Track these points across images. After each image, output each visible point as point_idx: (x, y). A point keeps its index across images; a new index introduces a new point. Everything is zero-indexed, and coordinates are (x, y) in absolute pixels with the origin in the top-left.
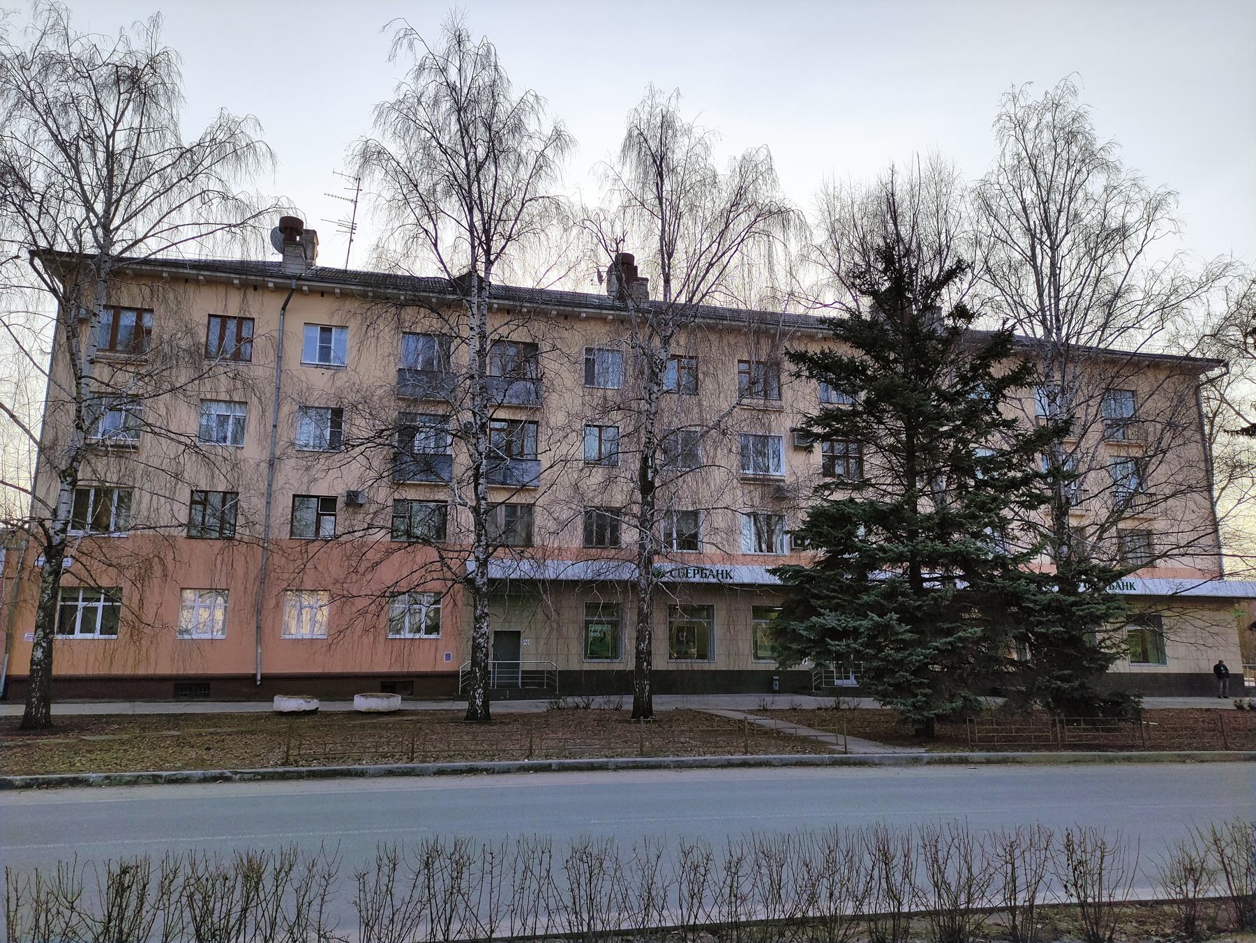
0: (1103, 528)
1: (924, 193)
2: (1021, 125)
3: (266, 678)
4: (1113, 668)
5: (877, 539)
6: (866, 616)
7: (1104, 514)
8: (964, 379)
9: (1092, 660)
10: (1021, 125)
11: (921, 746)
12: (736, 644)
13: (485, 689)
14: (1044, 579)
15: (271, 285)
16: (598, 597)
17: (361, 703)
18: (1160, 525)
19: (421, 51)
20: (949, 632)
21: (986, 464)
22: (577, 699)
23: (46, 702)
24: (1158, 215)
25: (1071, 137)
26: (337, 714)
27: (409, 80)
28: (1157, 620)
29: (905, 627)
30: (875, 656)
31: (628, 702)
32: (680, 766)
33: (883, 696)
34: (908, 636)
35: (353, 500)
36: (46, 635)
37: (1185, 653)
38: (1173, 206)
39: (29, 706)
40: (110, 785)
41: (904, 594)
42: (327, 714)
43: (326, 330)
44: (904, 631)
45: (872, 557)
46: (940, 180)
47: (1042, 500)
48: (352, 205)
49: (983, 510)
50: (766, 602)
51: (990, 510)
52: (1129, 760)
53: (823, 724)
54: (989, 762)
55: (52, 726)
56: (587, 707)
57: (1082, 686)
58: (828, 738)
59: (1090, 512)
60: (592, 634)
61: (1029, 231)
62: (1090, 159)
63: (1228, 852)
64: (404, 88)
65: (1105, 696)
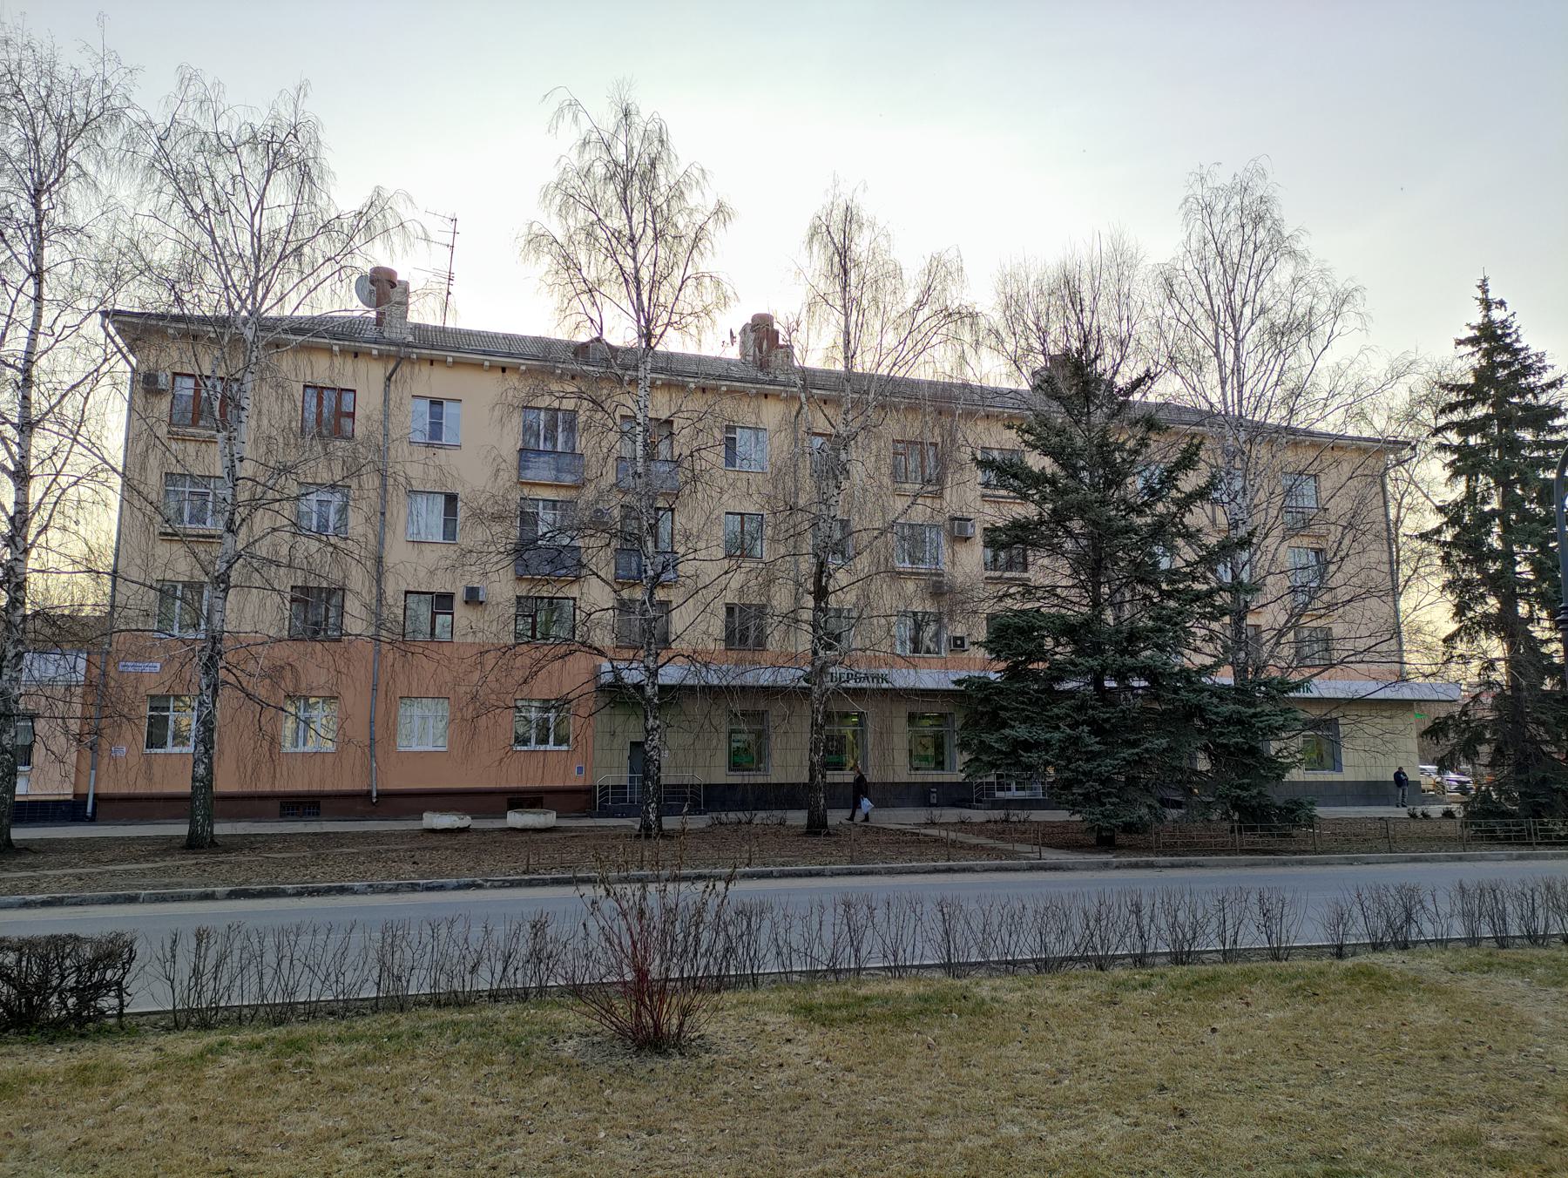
0: (1281, 633)
1: (1105, 276)
2: (1208, 208)
3: (385, 795)
4: (1288, 777)
5: (1064, 652)
6: (1057, 728)
7: (1282, 618)
8: (1152, 492)
9: (1270, 769)
10: (1208, 208)
11: (1106, 852)
12: (891, 756)
13: (658, 803)
14: (1220, 693)
15: (375, 352)
16: (753, 706)
17: (515, 819)
18: (1338, 630)
19: (585, 125)
20: (1135, 744)
21: (1172, 575)
22: (740, 814)
23: (210, 819)
24: (1345, 308)
25: (1258, 220)
26: (494, 830)
27: (574, 155)
28: (1332, 724)
29: (1094, 739)
30: (1066, 767)
31: (798, 818)
32: (890, 872)
33: (1073, 806)
34: (1096, 748)
35: (473, 597)
36: (207, 751)
37: (1361, 760)
38: (1359, 301)
39: (193, 823)
40: (373, 892)
41: (1093, 708)
42: (484, 832)
43: (436, 403)
44: (1093, 743)
45: (1063, 670)
46: (1122, 262)
47: (1223, 612)
48: (448, 251)
49: (1169, 629)
50: (919, 708)
51: (1176, 624)
52: (1301, 863)
53: (1000, 835)
54: (1173, 866)
55: (216, 845)
56: (750, 822)
57: (1260, 793)
58: (1019, 847)
59: (1268, 617)
60: (735, 745)
61: (1213, 316)
62: (1280, 246)
63: (1367, 903)
64: (564, 161)
65: (1279, 803)
